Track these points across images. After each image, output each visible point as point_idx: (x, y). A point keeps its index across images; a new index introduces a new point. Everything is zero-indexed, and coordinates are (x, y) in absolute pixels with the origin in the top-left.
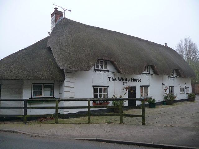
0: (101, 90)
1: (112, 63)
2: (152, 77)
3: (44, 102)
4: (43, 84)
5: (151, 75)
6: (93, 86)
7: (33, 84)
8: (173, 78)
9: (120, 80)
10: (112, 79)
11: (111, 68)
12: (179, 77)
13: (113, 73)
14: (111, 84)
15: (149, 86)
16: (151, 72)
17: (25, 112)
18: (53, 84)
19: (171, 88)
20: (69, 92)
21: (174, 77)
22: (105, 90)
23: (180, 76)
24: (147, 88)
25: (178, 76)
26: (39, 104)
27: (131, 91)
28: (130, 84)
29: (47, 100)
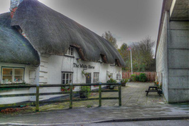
0: (67, 75)
1: (78, 50)
2: (101, 65)
3: (13, 90)
4: (14, 67)
5: (101, 63)
6: (62, 72)
7: (3, 68)
8: (113, 67)
9: (81, 67)
10: (76, 65)
11: (75, 55)
12: (117, 66)
13: (77, 59)
14: (75, 70)
15: (99, 73)
16: (101, 61)
17: (100, 95)
18: (23, 69)
19: (66, 75)
20: (43, 77)
21: (113, 66)
22: (70, 75)
23: (118, 66)
24: (70, 75)
25: (117, 65)
26: (9, 91)
27: (88, 76)
28: (88, 71)
29: (24, 86)
